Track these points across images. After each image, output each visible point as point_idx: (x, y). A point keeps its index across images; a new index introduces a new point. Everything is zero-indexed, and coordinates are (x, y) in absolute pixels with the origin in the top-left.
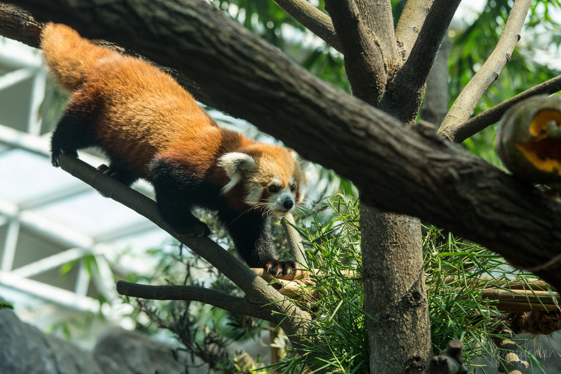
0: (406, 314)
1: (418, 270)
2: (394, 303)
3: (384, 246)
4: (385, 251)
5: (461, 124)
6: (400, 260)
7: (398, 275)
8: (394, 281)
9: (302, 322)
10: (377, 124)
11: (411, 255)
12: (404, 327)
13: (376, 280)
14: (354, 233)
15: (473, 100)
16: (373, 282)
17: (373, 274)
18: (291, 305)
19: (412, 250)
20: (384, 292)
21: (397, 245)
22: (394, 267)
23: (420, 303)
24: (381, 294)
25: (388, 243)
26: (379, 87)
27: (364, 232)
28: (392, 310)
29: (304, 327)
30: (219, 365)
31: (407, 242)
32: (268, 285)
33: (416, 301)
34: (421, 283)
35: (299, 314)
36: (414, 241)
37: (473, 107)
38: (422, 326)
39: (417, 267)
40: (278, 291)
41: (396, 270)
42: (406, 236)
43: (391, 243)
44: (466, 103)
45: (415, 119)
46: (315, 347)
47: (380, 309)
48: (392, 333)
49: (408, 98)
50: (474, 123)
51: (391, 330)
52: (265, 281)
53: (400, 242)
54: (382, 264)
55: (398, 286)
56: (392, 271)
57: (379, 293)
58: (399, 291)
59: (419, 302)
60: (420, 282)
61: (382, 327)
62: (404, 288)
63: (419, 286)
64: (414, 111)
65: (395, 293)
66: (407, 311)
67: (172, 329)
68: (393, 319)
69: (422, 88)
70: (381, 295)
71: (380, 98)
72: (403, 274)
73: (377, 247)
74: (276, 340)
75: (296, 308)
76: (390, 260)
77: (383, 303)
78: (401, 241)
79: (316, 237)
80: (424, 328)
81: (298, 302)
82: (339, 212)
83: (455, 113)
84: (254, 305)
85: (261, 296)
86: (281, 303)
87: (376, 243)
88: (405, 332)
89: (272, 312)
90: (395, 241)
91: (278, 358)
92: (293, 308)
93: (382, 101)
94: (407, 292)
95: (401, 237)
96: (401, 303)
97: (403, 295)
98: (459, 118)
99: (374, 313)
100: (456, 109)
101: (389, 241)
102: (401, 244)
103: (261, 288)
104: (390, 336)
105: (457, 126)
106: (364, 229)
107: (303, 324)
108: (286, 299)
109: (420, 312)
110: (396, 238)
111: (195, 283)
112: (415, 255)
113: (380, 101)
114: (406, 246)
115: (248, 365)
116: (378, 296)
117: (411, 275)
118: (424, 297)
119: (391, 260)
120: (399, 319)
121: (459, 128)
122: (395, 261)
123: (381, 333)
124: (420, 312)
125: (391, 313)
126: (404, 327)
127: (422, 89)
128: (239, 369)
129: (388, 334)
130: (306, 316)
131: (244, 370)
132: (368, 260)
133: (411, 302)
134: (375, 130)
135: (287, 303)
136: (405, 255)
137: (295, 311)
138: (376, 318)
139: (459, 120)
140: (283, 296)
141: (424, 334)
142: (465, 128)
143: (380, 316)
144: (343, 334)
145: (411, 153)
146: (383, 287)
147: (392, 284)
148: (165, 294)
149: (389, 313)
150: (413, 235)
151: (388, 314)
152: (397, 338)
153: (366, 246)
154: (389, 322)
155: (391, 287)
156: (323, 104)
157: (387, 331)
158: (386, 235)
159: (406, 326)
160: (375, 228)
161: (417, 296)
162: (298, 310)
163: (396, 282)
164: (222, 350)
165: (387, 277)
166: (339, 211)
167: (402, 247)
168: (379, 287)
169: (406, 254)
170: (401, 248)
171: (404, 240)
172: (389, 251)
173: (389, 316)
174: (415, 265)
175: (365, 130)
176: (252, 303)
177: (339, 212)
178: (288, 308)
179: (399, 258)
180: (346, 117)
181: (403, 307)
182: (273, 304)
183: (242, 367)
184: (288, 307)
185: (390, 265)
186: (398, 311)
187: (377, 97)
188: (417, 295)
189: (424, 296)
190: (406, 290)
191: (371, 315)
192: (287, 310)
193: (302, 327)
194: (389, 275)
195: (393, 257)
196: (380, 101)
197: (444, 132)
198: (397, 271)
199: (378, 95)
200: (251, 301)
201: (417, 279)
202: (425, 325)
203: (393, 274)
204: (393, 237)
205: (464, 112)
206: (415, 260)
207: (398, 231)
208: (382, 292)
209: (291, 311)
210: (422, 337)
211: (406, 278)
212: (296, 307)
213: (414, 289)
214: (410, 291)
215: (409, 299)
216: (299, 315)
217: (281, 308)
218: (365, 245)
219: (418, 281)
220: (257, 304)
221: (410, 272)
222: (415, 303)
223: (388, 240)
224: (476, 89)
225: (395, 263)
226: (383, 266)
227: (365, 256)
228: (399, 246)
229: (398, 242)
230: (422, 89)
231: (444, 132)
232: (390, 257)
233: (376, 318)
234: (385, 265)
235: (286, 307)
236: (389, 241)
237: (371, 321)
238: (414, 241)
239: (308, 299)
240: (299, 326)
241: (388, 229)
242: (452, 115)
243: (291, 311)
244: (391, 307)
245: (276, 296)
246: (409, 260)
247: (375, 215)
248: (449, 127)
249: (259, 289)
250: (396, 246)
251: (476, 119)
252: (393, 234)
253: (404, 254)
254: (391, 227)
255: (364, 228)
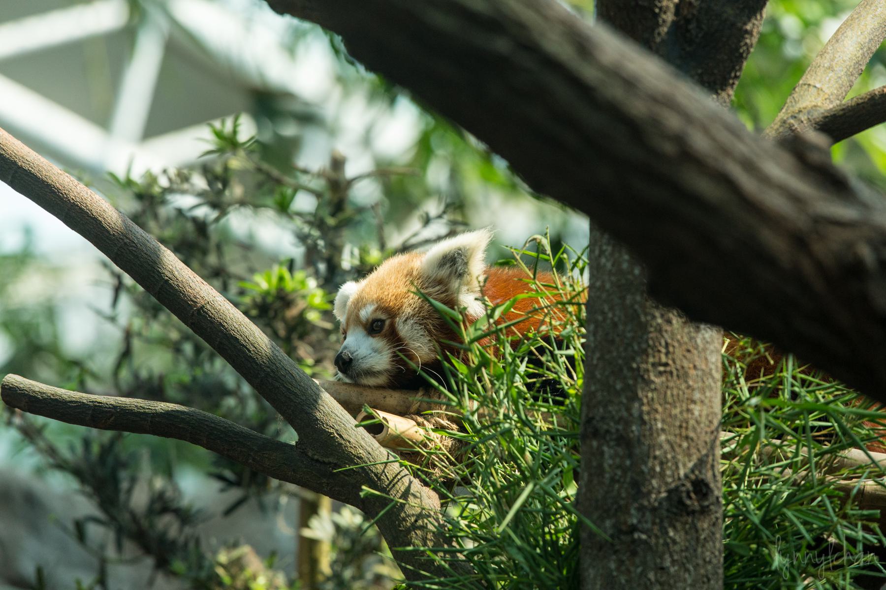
0: (675, 528)
1: (709, 430)
2: (649, 501)
3: (638, 369)
4: (640, 380)
5: (831, 106)
6: (670, 404)
7: (663, 437)
8: (654, 451)
9: (420, 516)
10: (706, 130)
11: (697, 396)
12: (667, 556)
13: (612, 443)
14: (565, 328)
15: (861, 51)
16: (605, 448)
17: (608, 431)
18: (402, 474)
19: (700, 384)
20: (629, 474)
21: (668, 369)
22: (655, 420)
23: (708, 506)
24: (621, 477)
25: (647, 363)
26: (661, 8)
27: (595, 334)
28: (643, 515)
29: (426, 528)
30: (178, 565)
31: (691, 366)
32: (356, 426)
33: (698, 501)
34: (713, 460)
35: (418, 495)
36: (707, 365)
37: (860, 67)
38: (708, 559)
39: (707, 423)
40: (375, 438)
41: (659, 425)
42: (689, 351)
43: (654, 365)
44: (845, 58)
45: (732, 88)
46: (454, 579)
47: (616, 510)
48: (638, 567)
49: (724, 39)
50: (864, 107)
51: (637, 560)
52: (346, 412)
53: (674, 362)
54: (628, 409)
55: (662, 464)
56: (651, 429)
57: (616, 474)
58: (662, 475)
59: (706, 503)
60: (711, 458)
61: (616, 552)
62: (674, 468)
63: (709, 466)
64: (733, 68)
65: (653, 477)
66: (677, 521)
67: (77, 472)
68: (644, 537)
69: (756, 19)
70: (622, 480)
71: (659, 34)
72: (675, 435)
73: (621, 370)
74: (314, 522)
75: (411, 482)
76: (648, 403)
77: (623, 499)
78: (678, 362)
79: (476, 330)
80: (710, 562)
81: (418, 469)
82: (534, 278)
83: (818, 78)
84: (318, 465)
85: (336, 446)
86: (380, 468)
87: (620, 362)
88: (668, 568)
89: (362, 490)
90: (664, 359)
91: (313, 563)
92: (406, 481)
93: (663, 41)
94: (679, 479)
95: (679, 352)
96: (664, 503)
97: (670, 484)
98: (828, 91)
99: (602, 519)
100: (822, 69)
101: (651, 360)
102: (677, 370)
103: (336, 427)
104: (633, 575)
105: (822, 110)
106: (596, 327)
107: (426, 521)
108: (391, 459)
109: (705, 525)
110: (667, 354)
111: (144, 374)
112: (706, 397)
113: (658, 40)
114: (686, 375)
115: (248, 572)
116: (613, 480)
117: (692, 439)
118: (716, 493)
119: (651, 403)
120: (657, 537)
121: (826, 114)
122: (661, 405)
123: (613, 566)
124: (705, 525)
125: (639, 522)
126: (667, 556)
127: (756, 22)
128: (226, 579)
129: (629, 571)
130: (429, 499)
131: (239, 583)
132: (599, 396)
133: (688, 502)
134: (700, 142)
135: (395, 468)
136: (684, 393)
137: (409, 488)
138: (604, 531)
139: (827, 96)
140: (384, 451)
141: (710, 576)
142: (840, 116)
143: (614, 526)
144: (526, 558)
145: (775, 201)
146: (628, 463)
147: (649, 457)
148: (113, 418)
149: (635, 521)
150: (705, 350)
151: (633, 525)
152: (649, 580)
153: (596, 366)
154: (634, 541)
155: (645, 463)
156: (589, 73)
157: (627, 562)
158: (644, 346)
159: (671, 556)
160: (621, 327)
161: (701, 490)
162: (417, 485)
163: (658, 453)
164: (188, 530)
165: (639, 440)
166: (534, 275)
167: (678, 376)
168: (618, 460)
169: (686, 391)
170: (675, 378)
171: (685, 361)
172: (648, 382)
173: (634, 529)
174: (703, 419)
175: (680, 140)
176: (312, 459)
177: (534, 278)
178: (396, 480)
179: (670, 400)
180: (638, 108)
181: (668, 510)
182: (362, 468)
183: (233, 577)
184: (394, 478)
185: (648, 413)
186: (658, 521)
187: (653, 30)
188: (701, 488)
189: (719, 490)
190: (679, 474)
191: (594, 523)
192: (393, 483)
193: (423, 528)
194: (644, 436)
195: (655, 396)
196: (658, 40)
197: (792, 121)
198: (663, 430)
199: (658, 25)
200: (310, 454)
201: (704, 452)
202: (713, 556)
203: (651, 434)
204: (659, 351)
205: (840, 78)
206: (705, 408)
207: (672, 339)
208: (625, 471)
209: (401, 487)
210: (704, 583)
211: (680, 446)
212: (412, 478)
213: (697, 472)
214: (686, 476)
215: (684, 495)
216: (417, 497)
217: (379, 479)
218: (595, 362)
219: (707, 456)
220: (324, 463)
221: (692, 434)
222: (696, 504)
223: (647, 356)
224: (869, 28)
225: (660, 409)
226: (631, 415)
227: (593, 388)
228: (671, 373)
229: (670, 362)
230: (756, 22)
231: (792, 121)
232: (650, 395)
233: (604, 531)
234: (635, 412)
235: (390, 478)
236: (651, 360)
237: (592, 535)
238: (707, 365)
239: (443, 466)
240: (414, 527)
241: (651, 332)
242: (811, 82)
243: (401, 487)
244: (641, 509)
245: (369, 449)
246: (692, 406)
247: (623, 298)
248: (805, 111)
249: (332, 431)
250: (665, 372)
251: (869, 99)
252: (660, 344)
253: (681, 393)
254: (658, 328)
255: (596, 322)
